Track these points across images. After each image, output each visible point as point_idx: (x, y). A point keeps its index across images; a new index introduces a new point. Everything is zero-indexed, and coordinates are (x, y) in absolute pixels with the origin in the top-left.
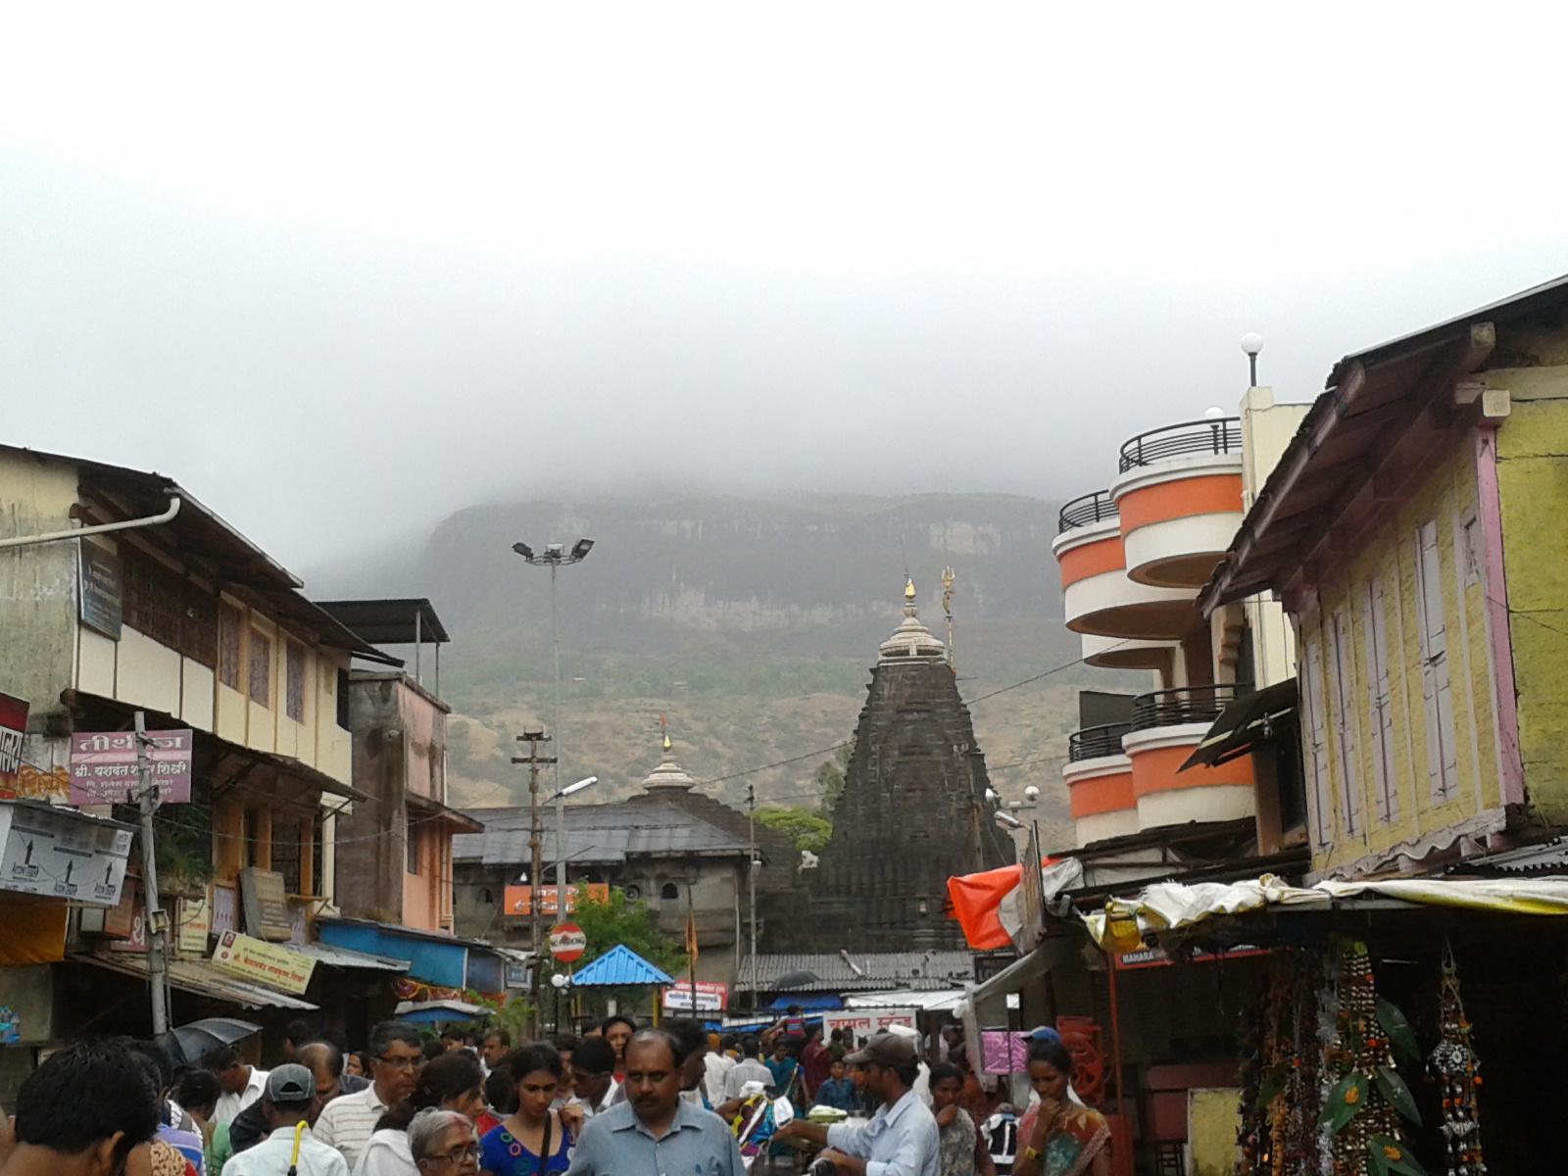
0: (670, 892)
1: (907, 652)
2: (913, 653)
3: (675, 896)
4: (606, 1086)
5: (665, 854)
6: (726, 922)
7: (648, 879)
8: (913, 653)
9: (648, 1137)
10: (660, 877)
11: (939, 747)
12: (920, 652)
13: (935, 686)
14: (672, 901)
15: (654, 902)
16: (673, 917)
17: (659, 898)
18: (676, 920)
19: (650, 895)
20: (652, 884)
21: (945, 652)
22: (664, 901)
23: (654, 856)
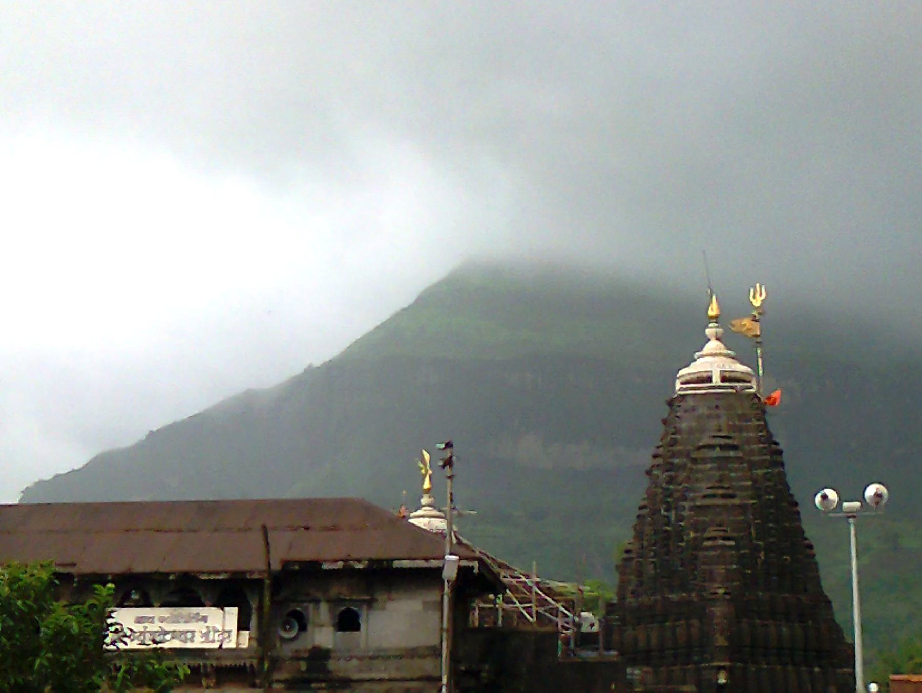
0: (348, 622)
1: (709, 380)
2: (716, 380)
3: (356, 627)
4: (503, 622)
5: (340, 565)
6: (427, 666)
7: (317, 602)
8: (716, 380)
9: (59, 565)
10: (334, 602)
11: (746, 488)
12: (724, 379)
13: (742, 417)
14: (349, 634)
15: (323, 636)
16: (351, 658)
17: (332, 629)
18: (355, 662)
19: (322, 626)
20: (324, 607)
21: (754, 384)
22: (340, 633)
23: (325, 566)
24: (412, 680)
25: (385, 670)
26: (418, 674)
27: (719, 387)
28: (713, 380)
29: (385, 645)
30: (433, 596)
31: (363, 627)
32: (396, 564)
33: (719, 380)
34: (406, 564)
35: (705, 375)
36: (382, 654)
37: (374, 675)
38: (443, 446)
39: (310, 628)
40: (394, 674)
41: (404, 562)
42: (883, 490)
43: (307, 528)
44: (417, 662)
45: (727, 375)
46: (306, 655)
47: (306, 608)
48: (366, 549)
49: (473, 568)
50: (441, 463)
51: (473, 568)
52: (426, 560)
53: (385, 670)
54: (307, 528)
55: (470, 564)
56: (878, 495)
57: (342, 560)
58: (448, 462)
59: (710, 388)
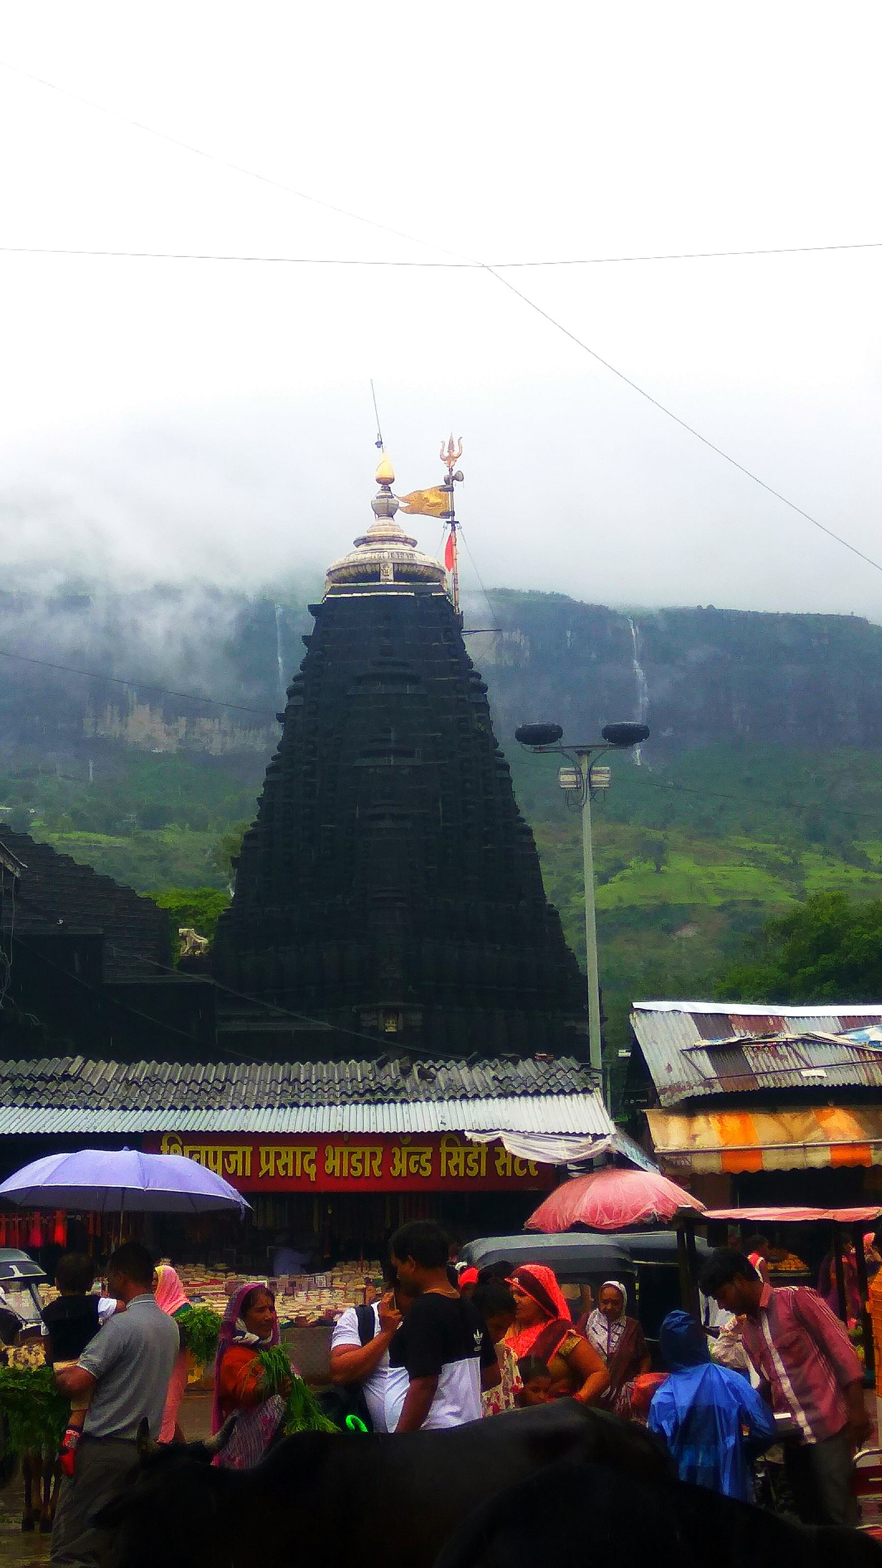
1: (376, 576)
2: (388, 577)
8: (388, 577)
12: (398, 576)
33: (391, 577)
35: (369, 569)
45: (405, 569)
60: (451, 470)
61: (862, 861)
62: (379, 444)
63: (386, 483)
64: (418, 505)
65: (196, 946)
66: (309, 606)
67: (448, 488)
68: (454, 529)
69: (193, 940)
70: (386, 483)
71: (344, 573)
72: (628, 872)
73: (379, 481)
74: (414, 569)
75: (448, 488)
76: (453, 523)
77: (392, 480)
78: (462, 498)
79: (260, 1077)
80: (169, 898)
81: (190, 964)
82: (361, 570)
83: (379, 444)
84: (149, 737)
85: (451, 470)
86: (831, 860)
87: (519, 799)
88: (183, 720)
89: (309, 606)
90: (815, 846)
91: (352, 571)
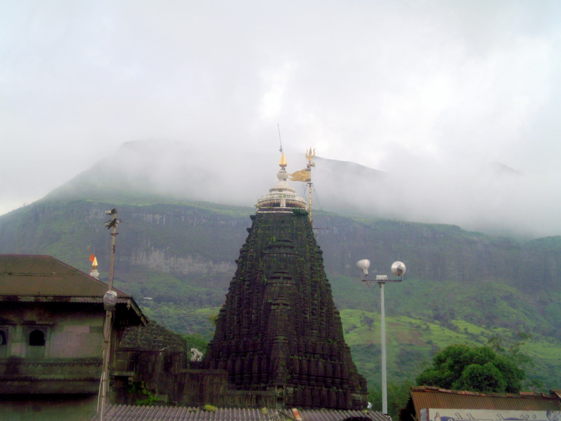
0: (37, 339)
1: (278, 204)
2: (283, 205)
5: (32, 299)
8: (283, 205)
14: (36, 348)
17: (24, 344)
22: (30, 347)
24: (80, 380)
25: (62, 373)
26: (84, 376)
27: (285, 210)
28: (281, 205)
29: (62, 356)
30: (97, 323)
31: (47, 343)
32: (73, 300)
33: (285, 205)
34: (79, 300)
35: (276, 201)
36: (59, 362)
37: (52, 376)
38: (110, 212)
39: (9, 342)
40: (67, 377)
41: (77, 298)
42: (403, 265)
43: (10, 274)
44: (84, 369)
45: (290, 202)
46: (6, 361)
47: (7, 330)
48: (51, 288)
49: (126, 304)
50: (108, 224)
51: (126, 304)
52: (93, 297)
53: (62, 373)
54: (10, 274)
55: (125, 302)
56: (400, 270)
57: (34, 296)
58: (113, 224)
59: (277, 210)
60: (310, 162)
61: (455, 329)
62: (281, 150)
63: (283, 166)
64: (297, 177)
65: (198, 356)
66: (251, 216)
67: (308, 170)
68: (310, 186)
69: (197, 355)
70: (283, 166)
71: (265, 202)
72: (357, 329)
73: (280, 165)
74: (294, 202)
75: (308, 170)
76: (310, 184)
77: (286, 166)
78: (315, 175)
79: (259, 368)
80: (187, 334)
81: (194, 365)
82: (272, 201)
83: (281, 150)
84: (158, 266)
85: (310, 162)
86: (443, 328)
87: (334, 300)
88: (172, 259)
89: (251, 216)
90: (437, 322)
91: (269, 202)
